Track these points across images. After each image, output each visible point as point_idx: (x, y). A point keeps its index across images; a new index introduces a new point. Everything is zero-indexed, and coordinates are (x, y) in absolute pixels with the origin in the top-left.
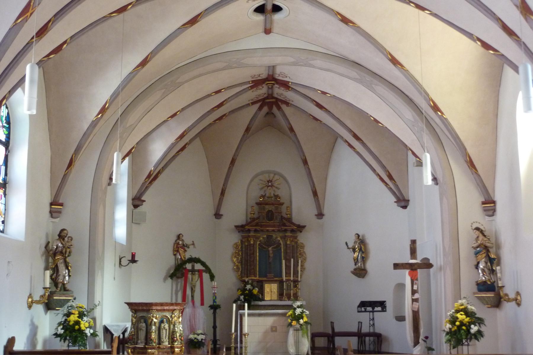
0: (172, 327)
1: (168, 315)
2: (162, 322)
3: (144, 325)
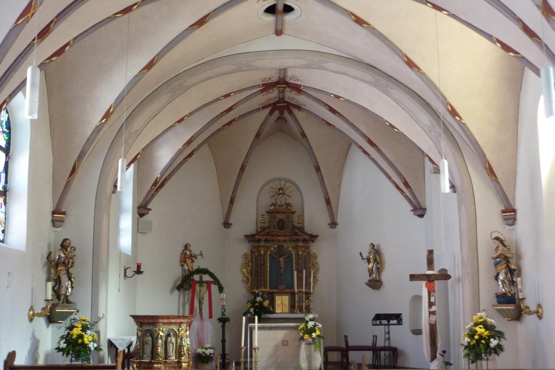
0: (179, 340)
1: (175, 328)
2: (168, 335)
3: (150, 338)
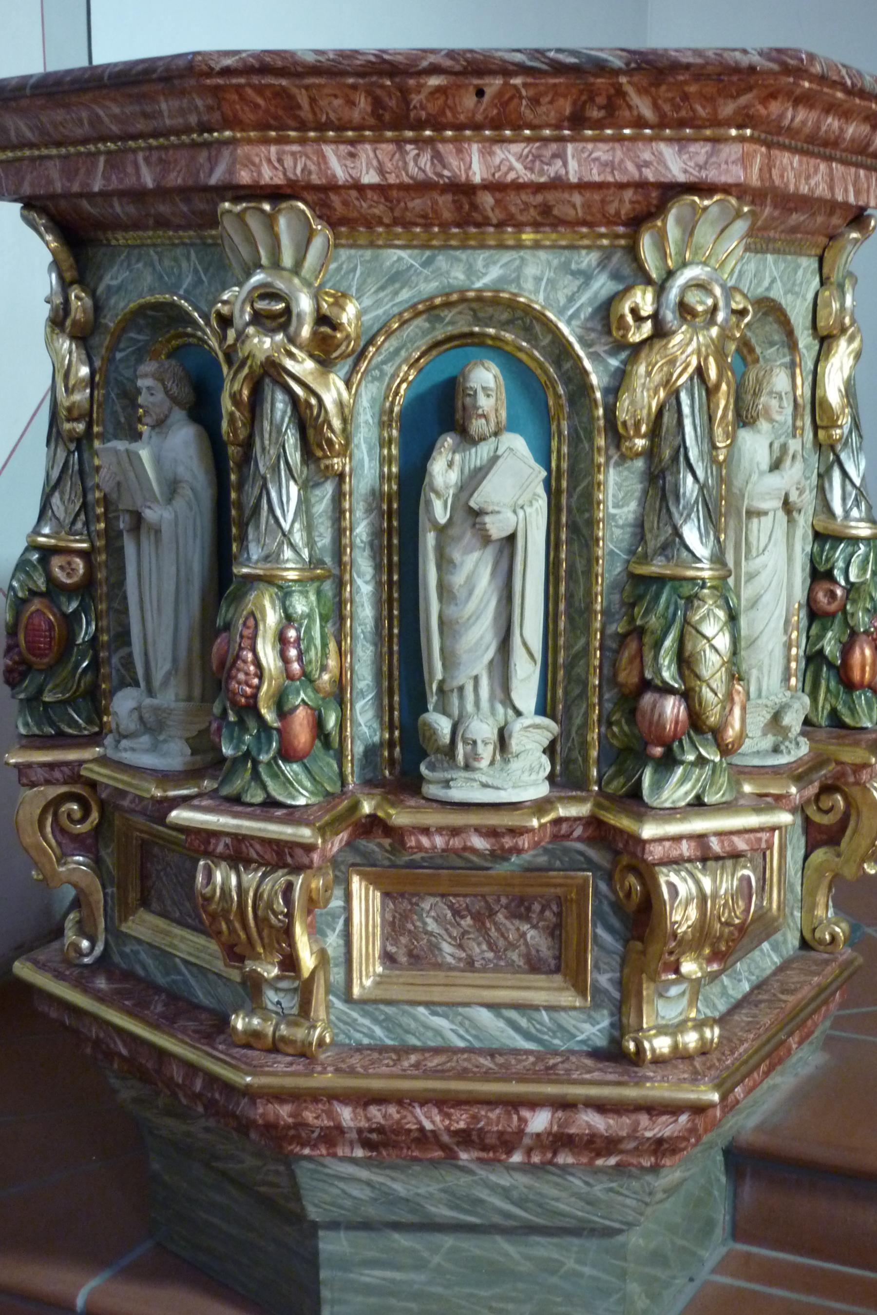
0: (618, 495)
1: (553, 283)
2: (440, 413)
3: (182, 441)
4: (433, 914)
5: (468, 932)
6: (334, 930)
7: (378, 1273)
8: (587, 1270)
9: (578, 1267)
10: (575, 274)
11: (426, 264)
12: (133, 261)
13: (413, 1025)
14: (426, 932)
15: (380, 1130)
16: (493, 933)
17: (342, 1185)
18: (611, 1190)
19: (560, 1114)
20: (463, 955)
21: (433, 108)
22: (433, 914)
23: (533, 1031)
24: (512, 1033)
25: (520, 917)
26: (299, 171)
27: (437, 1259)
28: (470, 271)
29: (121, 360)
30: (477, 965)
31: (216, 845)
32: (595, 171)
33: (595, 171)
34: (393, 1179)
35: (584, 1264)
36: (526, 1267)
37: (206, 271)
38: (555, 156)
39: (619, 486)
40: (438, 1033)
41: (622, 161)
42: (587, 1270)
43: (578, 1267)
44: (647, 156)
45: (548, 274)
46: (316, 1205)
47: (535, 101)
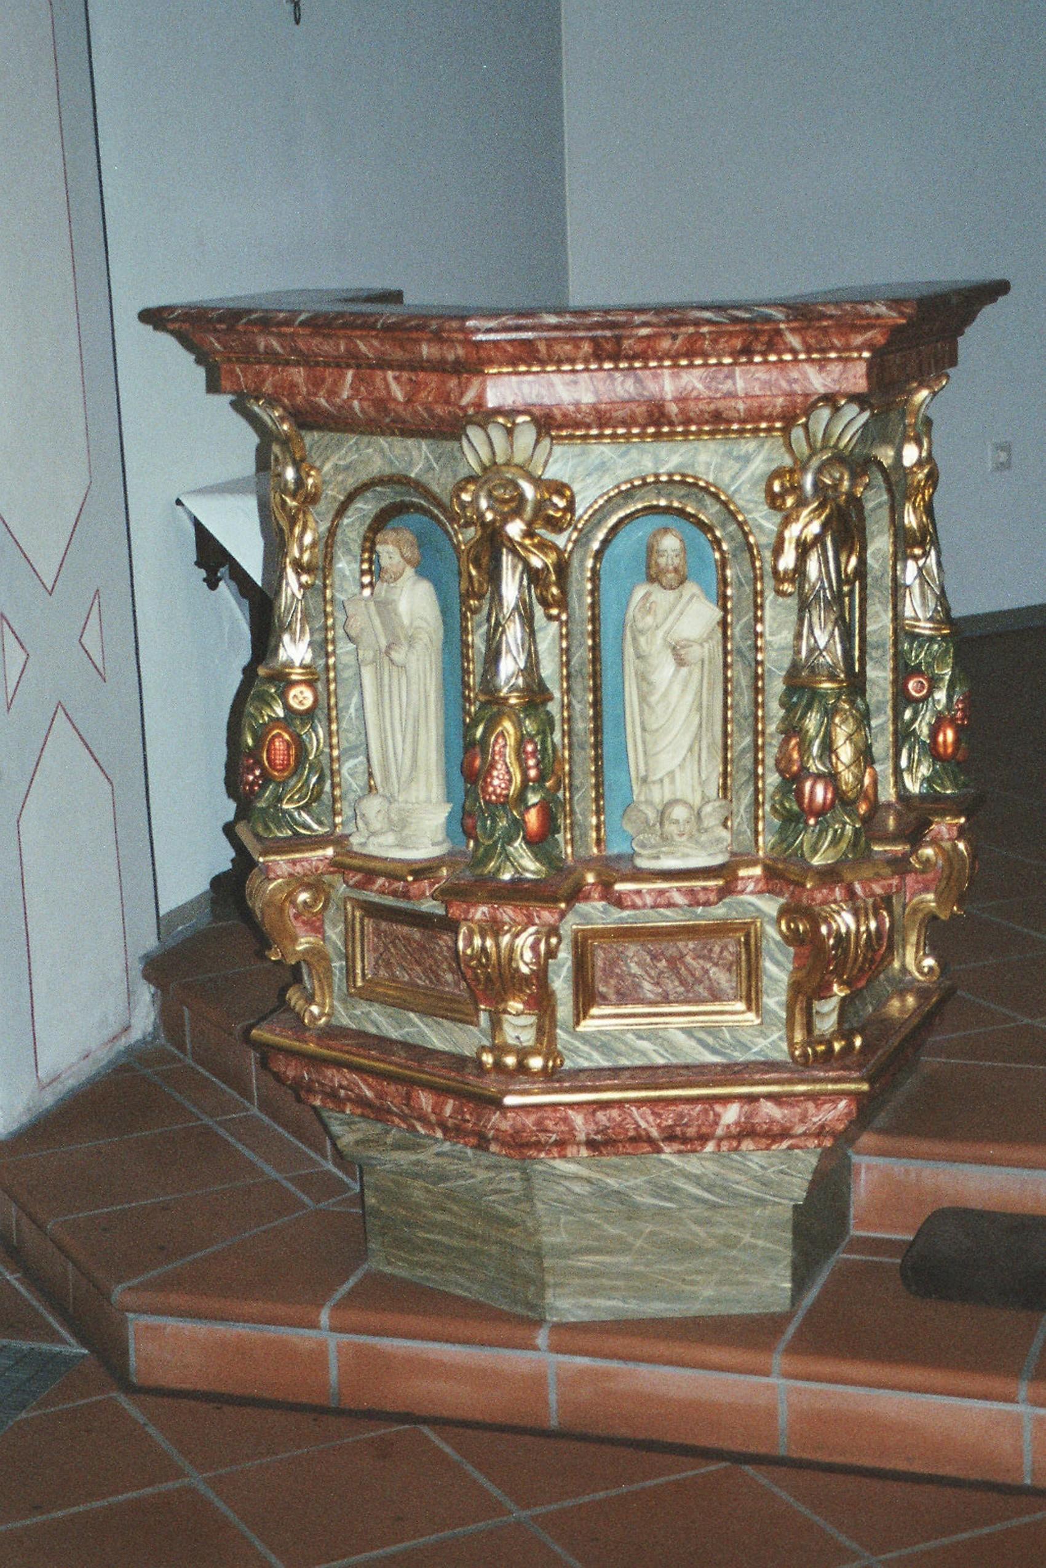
4: (636, 959)
5: (663, 972)
6: (559, 977)
7: (591, 1258)
8: (760, 1243)
9: (753, 1240)
10: (738, 458)
11: (623, 455)
12: (362, 446)
13: (624, 1048)
14: (630, 974)
15: (603, 1131)
16: (683, 971)
17: (567, 1183)
18: (781, 1172)
19: (746, 1107)
20: (660, 990)
21: (638, 348)
22: (636, 959)
23: (717, 1046)
24: (701, 1049)
25: (703, 957)
26: (534, 396)
27: (639, 1243)
28: (657, 461)
29: (347, 525)
30: (671, 998)
31: (474, 914)
32: (756, 389)
33: (756, 389)
34: (607, 1175)
35: (759, 1238)
36: (712, 1243)
37: (437, 460)
38: (727, 377)
39: (774, 619)
40: (643, 1053)
41: (777, 380)
42: (760, 1243)
43: (753, 1240)
44: (795, 375)
45: (716, 460)
46: (544, 1203)
47: (715, 341)
